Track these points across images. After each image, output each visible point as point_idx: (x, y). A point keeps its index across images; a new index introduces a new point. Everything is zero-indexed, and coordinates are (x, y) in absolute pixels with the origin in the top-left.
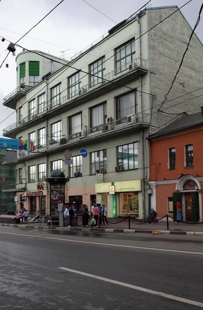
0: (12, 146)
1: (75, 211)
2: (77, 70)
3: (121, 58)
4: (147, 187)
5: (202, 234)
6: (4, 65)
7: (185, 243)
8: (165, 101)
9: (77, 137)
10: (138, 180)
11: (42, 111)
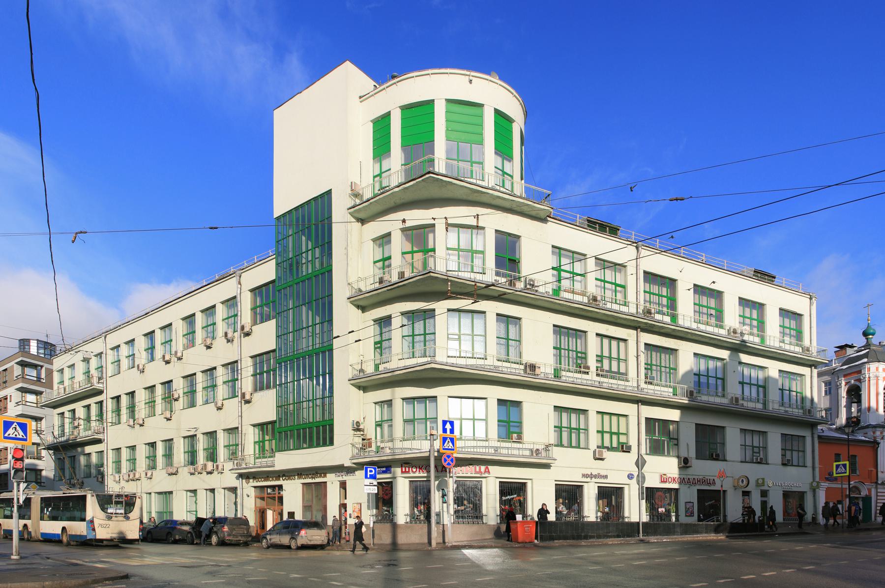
0: (444, 423)
1: (715, 502)
2: (505, 161)
3: (383, 171)
4: (487, 470)
5: (1, 583)
6: (670, 235)
7: (164, 464)
8: (657, 253)
9: (645, 301)
10: (503, 428)
11: (316, 321)
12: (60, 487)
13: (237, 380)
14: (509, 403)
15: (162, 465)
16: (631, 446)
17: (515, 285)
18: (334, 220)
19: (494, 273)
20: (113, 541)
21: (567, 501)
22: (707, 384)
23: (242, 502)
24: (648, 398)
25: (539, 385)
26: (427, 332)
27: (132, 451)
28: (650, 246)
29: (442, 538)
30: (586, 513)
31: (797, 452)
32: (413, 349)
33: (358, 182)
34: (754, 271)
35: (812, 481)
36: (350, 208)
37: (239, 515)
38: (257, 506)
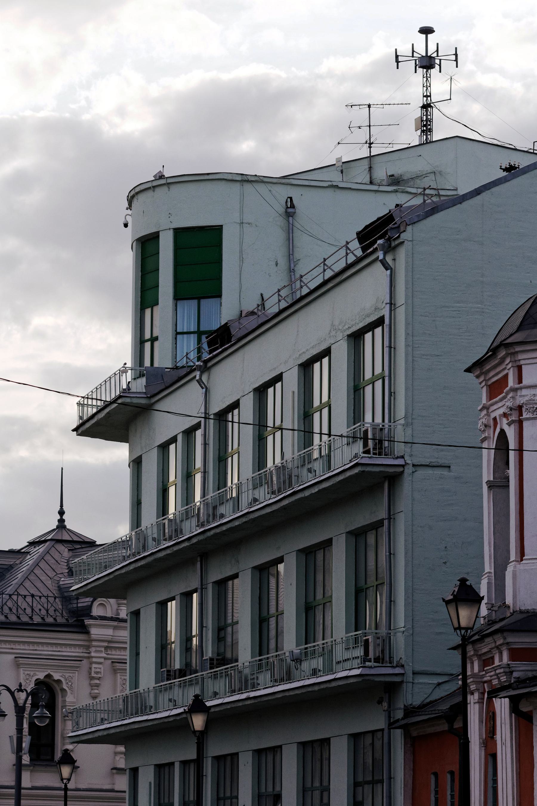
4: (348, 251)
7: (387, 515)
12: (30, 696)
13: (382, 781)
15: (406, 363)
17: (365, 664)
18: (61, 539)
24: (516, 783)
25: (200, 629)
26: (261, 427)
28: (106, 579)
29: (14, 778)
30: (419, 203)
31: (91, 400)
34: (315, 669)
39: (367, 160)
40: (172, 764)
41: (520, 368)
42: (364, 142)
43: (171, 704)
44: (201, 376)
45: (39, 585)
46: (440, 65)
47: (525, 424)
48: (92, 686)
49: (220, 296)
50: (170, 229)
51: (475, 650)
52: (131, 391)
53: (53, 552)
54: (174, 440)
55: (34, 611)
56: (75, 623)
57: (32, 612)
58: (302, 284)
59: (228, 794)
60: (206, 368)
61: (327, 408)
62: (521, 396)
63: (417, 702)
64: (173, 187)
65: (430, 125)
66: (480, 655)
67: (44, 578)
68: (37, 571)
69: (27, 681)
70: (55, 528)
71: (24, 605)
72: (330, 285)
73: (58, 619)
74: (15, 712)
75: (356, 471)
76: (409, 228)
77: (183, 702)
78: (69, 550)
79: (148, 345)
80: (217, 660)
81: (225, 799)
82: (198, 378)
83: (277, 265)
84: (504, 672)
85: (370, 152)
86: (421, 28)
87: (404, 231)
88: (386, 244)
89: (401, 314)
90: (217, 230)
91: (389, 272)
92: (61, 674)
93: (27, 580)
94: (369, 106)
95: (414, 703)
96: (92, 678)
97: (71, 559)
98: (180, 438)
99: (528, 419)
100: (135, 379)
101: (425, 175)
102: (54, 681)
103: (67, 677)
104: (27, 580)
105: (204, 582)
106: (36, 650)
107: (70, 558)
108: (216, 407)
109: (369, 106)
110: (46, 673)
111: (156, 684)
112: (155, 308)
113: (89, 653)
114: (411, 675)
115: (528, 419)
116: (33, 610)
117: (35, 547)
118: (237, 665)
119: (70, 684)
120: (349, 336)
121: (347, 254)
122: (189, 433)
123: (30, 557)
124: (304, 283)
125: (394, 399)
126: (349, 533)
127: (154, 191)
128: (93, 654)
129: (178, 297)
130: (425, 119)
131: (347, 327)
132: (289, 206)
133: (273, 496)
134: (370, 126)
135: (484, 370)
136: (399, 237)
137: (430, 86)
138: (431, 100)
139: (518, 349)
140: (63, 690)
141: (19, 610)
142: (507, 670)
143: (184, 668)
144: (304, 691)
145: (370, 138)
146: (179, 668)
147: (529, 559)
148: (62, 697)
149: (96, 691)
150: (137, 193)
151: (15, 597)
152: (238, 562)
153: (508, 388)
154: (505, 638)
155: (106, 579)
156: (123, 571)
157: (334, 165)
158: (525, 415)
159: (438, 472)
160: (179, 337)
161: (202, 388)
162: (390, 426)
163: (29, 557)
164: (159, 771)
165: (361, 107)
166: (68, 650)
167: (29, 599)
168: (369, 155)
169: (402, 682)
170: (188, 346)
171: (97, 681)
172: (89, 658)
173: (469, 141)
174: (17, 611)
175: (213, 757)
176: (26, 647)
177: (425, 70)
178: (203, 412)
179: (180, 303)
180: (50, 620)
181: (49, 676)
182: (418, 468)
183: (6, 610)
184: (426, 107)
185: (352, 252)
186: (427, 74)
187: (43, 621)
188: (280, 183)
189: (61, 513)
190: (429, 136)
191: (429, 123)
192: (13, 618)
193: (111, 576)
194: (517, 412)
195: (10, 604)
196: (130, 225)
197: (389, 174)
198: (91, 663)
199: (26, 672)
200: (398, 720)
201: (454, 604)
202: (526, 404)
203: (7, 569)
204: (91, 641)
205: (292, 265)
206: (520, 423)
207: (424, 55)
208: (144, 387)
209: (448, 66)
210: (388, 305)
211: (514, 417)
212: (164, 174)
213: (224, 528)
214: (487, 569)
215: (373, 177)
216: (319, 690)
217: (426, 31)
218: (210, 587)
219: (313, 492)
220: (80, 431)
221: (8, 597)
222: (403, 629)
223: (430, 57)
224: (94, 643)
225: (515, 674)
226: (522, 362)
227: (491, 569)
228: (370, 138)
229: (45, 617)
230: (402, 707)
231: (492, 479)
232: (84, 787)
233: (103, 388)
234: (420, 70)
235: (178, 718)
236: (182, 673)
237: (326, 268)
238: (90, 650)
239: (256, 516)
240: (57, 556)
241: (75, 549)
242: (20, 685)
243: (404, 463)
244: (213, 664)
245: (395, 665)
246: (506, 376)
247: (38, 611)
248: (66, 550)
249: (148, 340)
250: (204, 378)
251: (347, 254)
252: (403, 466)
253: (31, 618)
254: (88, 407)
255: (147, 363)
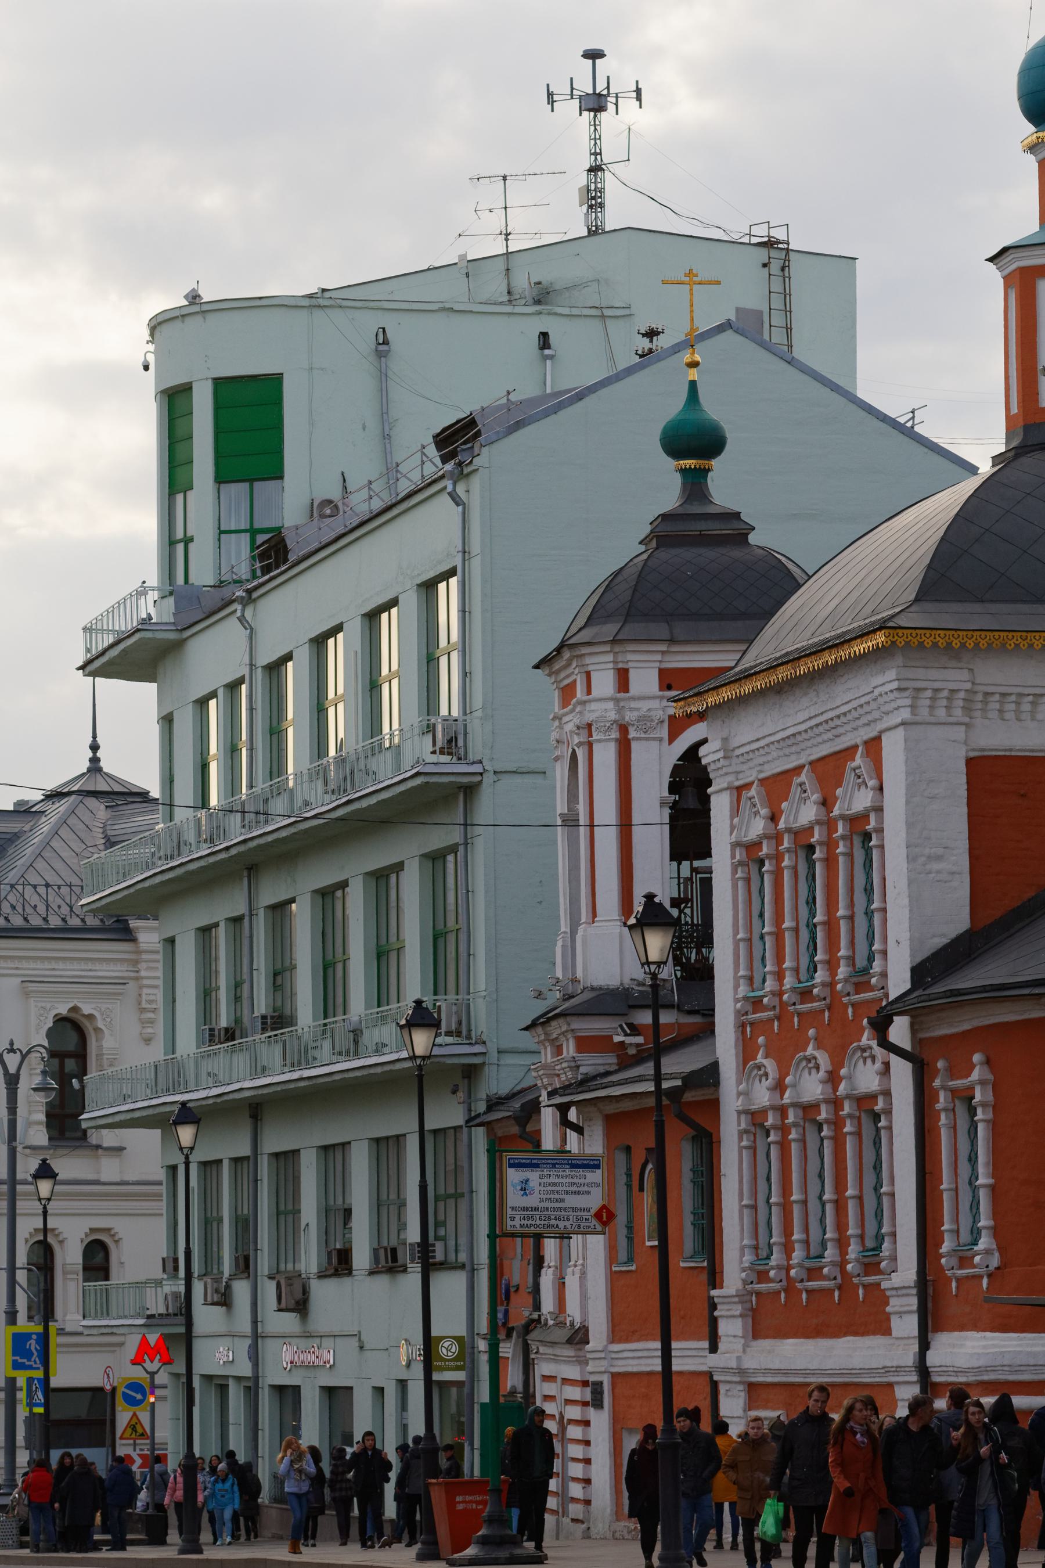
4: (425, 459)
6: (662, 342)
10: (219, 1308)
14: (291, 1389)
16: (738, 310)
18: (422, 1383)
19: (10, 1364)
20: (985, 1531)
21: (57, 1505)
22: (659, 1381)
23: (373, 635)
27: (579, 974)
28: (126, 893)
32: (507, 1305)
33: (178, 1547)
35: (730, 332)
36: (179, 834)
37: (652, 1077)
38: (334, 1444)
39: (502, 257)
40: (220, 1161)
41: (588, 674)
42: (499, 232)
43: (210, 1079)
44: (243, 611)
45: (58, 865)
46: (616, 104)
47: (595, 747)
48: (143, 1023)
49: (281, 477)
50: (207, 379)
51: (546, 1034)
52: (152, 621)
53: (81, 811)
54: (213, 695)
55: (50, 909)
56: (116, 925)
57: (47, 910)
58: (372, 493)
59: (290, 1207)
60: (249, 599)
61: (397, 679)
62: (590, 711)
63: (504, 1090)
64: (209, 316)
65: (600, 197)
66: (553, 1040)
67: (66, 854)
68: (56, 843)
69: (41, 1018)
70: (85, 771)
71: (34, 900)
72: (395, 511)
73: (87, 919)
74: (6, 1083)
75: (418, 781)
76: (485, 450)
77: (231, 1077)
78: (107, 807)
79: (180, 548)
80: (272, 1017)
81: (286, 1213)
82: (239, 614)
83: (364, 429)
84: (568, 1067)
85: (507, 247)
86: (584, 51)
87: (479, 455)
88: (456, 471)
89: (476, 565)
90: (276, 380)
91: (460, 508)
92: (93, 1006)
93: (40, 859)
94: (505, 178)
95: (499, 1093)
96: (143, 1010)
97: (109, 823)
98: (221, 693)
99: (599, 741)
100: (162, 598)
101: (585, 285)
102: (84, 1015)
103: (103, 1009)
104: (40, 859)
105: (254, 904)
106: (54, 969)
107: (108, 820)
108: (266, 657)
109: (505, 178)
110: (71, 1005)
111: (197, 1048)
112: (189, 494)
113: (137, 972)
114: (496, 1054)
115: (599, 741)
116: (48, 906)
117: (53, 803)
118: (296, 1030)
119: (108, 1020)
120: (419, 586)
121: (423, 463)
122: (234, 686)
123: (46, 819)
124: (375, 492)
125: (471, 681)
126: (424, 856)
127: (183, 322)
128: (143, 973)
129: (221, 478)
130: (593, 188)
131: (416, 573)
132: (381, 342)
133: (334, 797)
134: (506, 208)
135: (554, 670)
136: (471, 462)
137: (600, 139)
138: (602, 160)
139: (585, 650)
140: (97, 1030)
141: (27, 907)
142: (573, 1064)
143: (233, 1025)
144: (365, 1072)
145: (507, 226)
146: (225, 1026)
147: (602, 921)
148: (97, 1041)
149: (150, 1030)
150: (160, 324)
151: (20, 888)
152: (294, 881)
153: (574, 700)
154: (569, 1024)
155: (126, 893)
156: (147, 884)
157: (456, 264)
158: (595, 736)
159: (528, 780)
160: (222, 535)
161: (246, 629)
162: (466, 720)
163: (44, 819)
164: (205, 1171)
165: (492, 179)
166: (104, 968)
167: (42, 890)
168: (505, 252)
169: (484, 1064)
170: (238, 553)
171: (151, 1015)
172: (137, 979)
173: (648, 233)
174: (24, 909)
175: (270, 1154)
176: (39, 965)
177: (592, 114)
178: (248, 663)
179: (223, 486)
180: (75, 922)
181: (75, 1009)
182: (500, 776)
183: (6, 908)
184: (595, 169)
185: (430, 460)
186: (595, 121)
187: (63, 924)
188: (366, 308)
189: (95, 747)
190: (599, 215)
191: (599, 194)
192: (17, 921)
193: (132, 890)
194: (586, 731)
195: (12, 898)
196: (152, 367)
197: (533, 281)
198: (141, 987)
199: (40, 1005)
200: (478, 1116)
201: (407, 1030)
202: (596, 722)
203: (9, 839)
204: (139, 952)
205: (387, 428)
206: (590, 745)
207: (591, 91)
208: (172, 615)
209: (629, 105)
210: (460, 554)
211: (583, 738)
212: (200, 292)
213: (270, 838)
214: (563, 929)
215: (512, 285)
216: (382, 1072)
217: (593, 55)
218: (261, 912)
219: (372, 803)
220: (89, 669)
221: (8, 888)
222: (484, 993)
223: (600, 95)
224: (144, 956)
225: (582, 1070)
226: (590, 668)
227: (566, 927)
228: (507, 226)
229: (68, 918)
230: (484, 1097)
231: (566, 812)
232: (135, 1179)
233: (116, 611)
234: (585, 114)
235: (219, 1100)
236: (230, 1035)
237: (399, 476)
238: (139, 966)
239: (307, 827)
240: (86, 817)
241: (118, 805)
242: (12, 1044)
243: (482, 771)
244: (266, 1023)
245: (473, 1042)
246: (575, 681)
247: (56, 909)
248: (103, 807)
249: (180, 541)
250: (248, 613)
251: (423, 463)
252: (481, 774)
253: (45, 920)
254: (103, 634)
255: (180, 580)
